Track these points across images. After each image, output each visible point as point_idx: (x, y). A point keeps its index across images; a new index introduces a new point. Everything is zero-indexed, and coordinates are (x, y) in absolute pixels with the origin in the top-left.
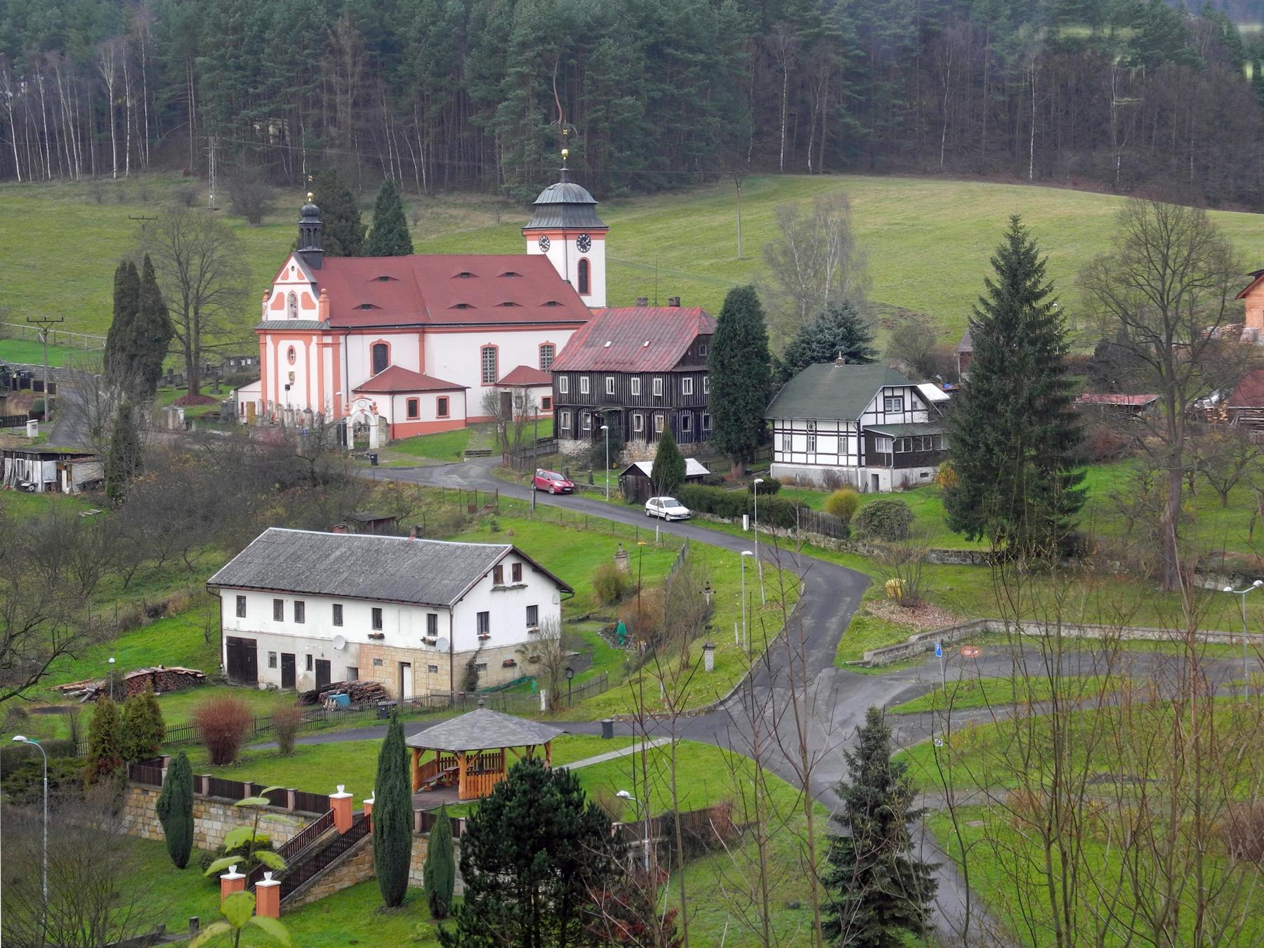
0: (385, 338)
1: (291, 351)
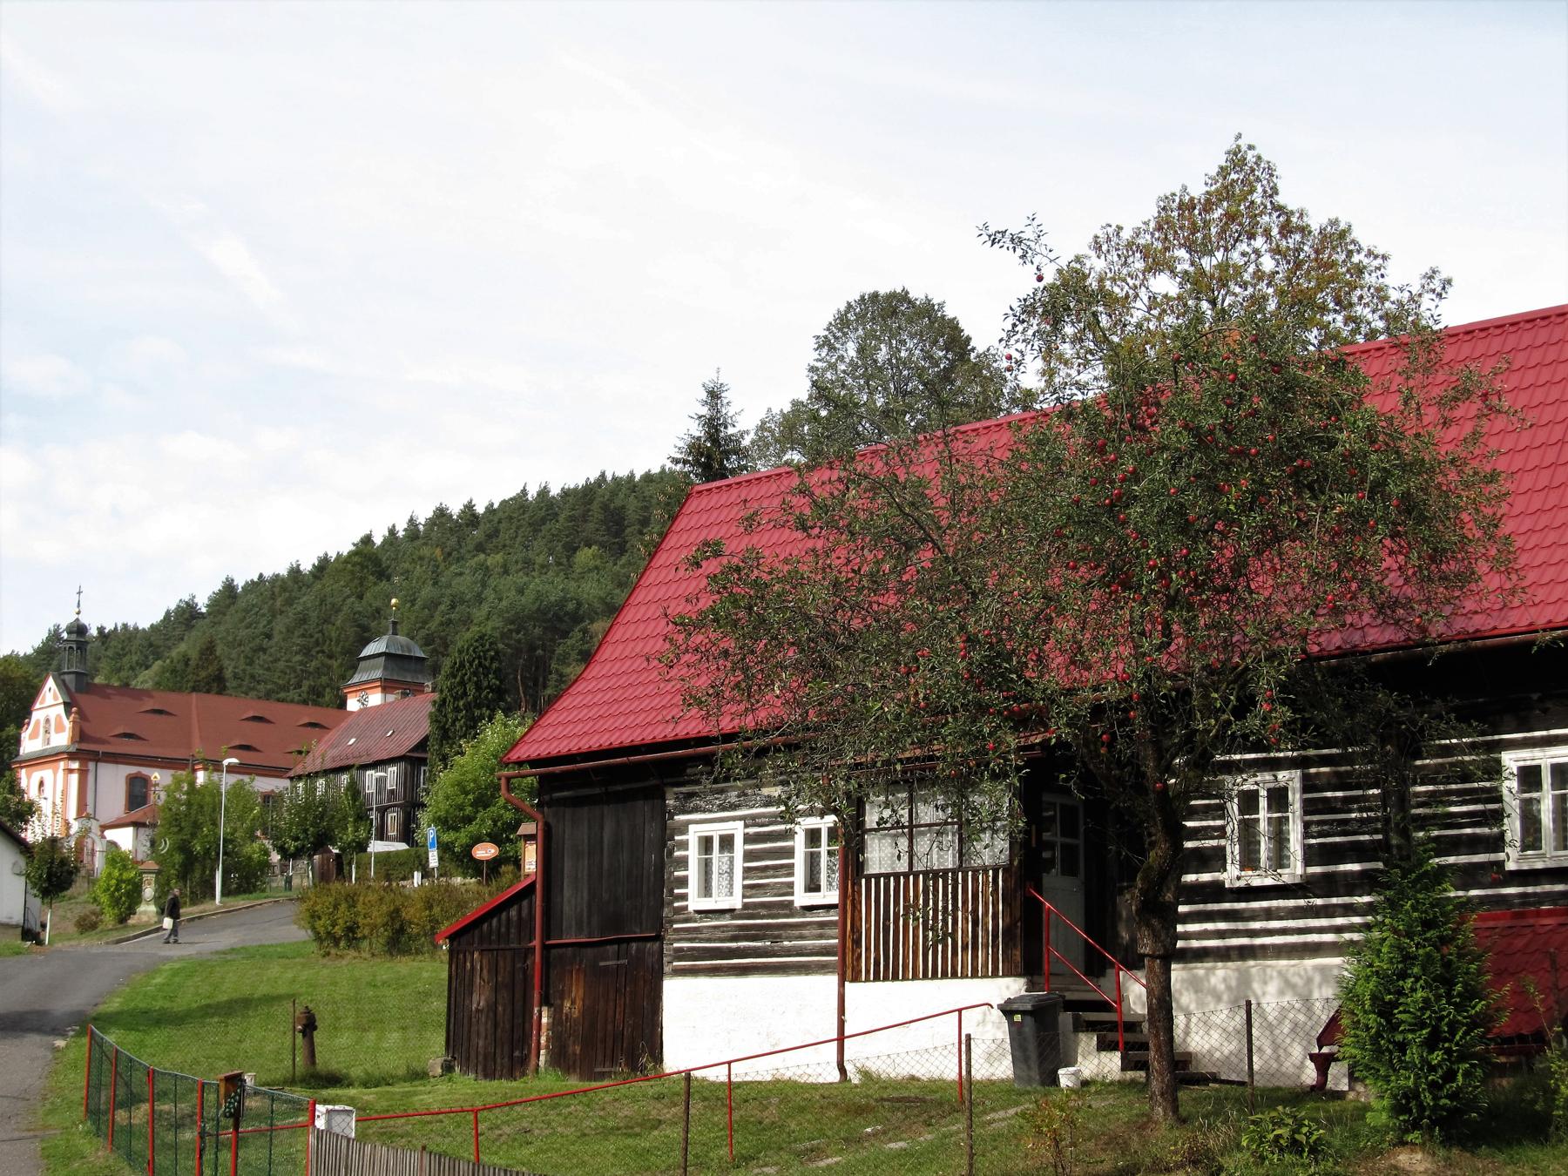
0: (145, 771)
1: (41, 784)
